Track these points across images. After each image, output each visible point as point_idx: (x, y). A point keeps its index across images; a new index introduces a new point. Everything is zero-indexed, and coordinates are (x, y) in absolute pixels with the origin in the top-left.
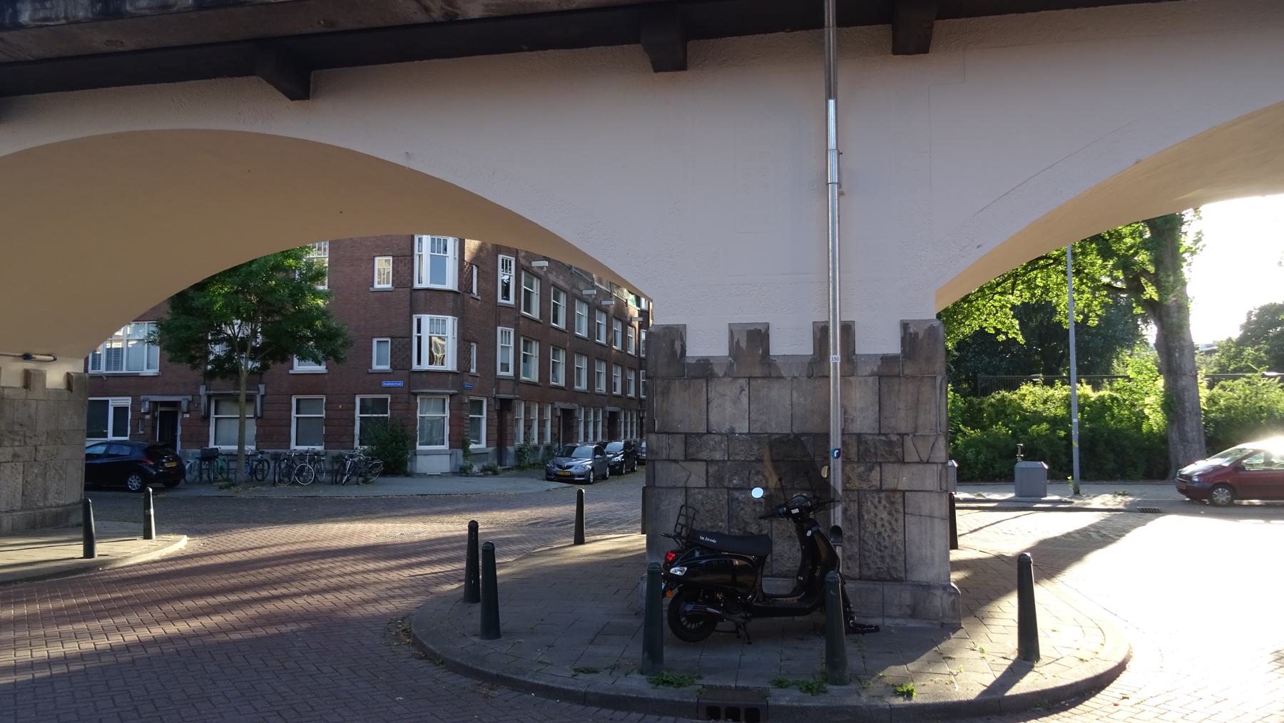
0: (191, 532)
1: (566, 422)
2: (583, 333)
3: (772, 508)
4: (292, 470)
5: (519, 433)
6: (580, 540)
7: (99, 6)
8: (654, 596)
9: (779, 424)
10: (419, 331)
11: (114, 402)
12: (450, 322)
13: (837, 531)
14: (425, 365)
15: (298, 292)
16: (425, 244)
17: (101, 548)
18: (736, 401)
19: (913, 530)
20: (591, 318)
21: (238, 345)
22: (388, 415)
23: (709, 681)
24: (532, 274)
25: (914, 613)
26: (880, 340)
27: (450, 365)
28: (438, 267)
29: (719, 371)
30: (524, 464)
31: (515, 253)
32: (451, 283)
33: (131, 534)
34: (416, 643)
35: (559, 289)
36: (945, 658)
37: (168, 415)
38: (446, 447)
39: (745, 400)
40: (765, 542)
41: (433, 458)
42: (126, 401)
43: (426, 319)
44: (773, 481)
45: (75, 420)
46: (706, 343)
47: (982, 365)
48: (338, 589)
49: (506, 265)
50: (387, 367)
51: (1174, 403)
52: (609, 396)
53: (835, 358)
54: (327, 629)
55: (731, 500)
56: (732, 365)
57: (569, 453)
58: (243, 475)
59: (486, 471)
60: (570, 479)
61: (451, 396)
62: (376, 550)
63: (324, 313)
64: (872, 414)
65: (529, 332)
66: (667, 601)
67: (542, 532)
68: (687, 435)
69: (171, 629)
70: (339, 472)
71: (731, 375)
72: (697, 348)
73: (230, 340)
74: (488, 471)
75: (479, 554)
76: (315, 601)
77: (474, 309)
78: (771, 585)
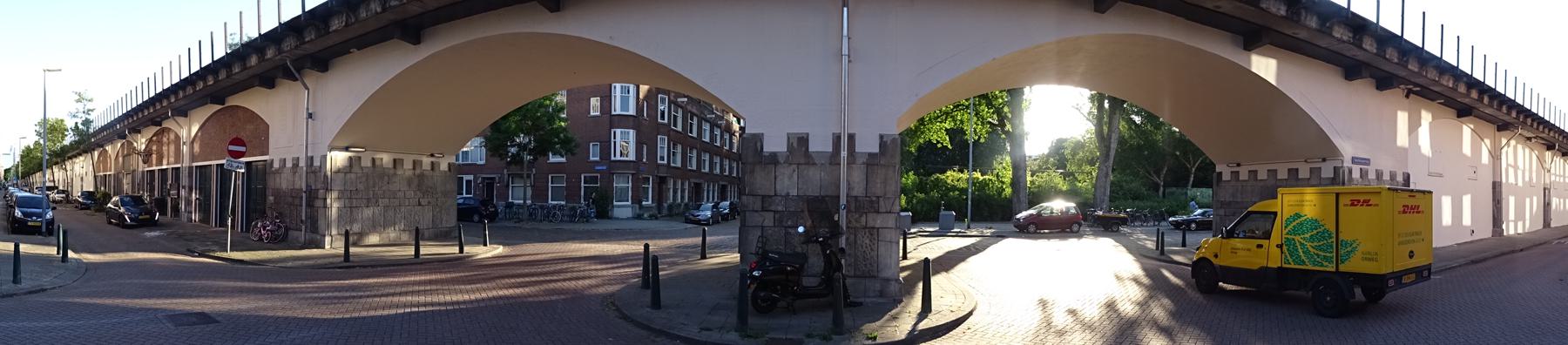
0: (504, 244)
1: (697, 192)
2: (707, 139)
3: (808, 238)
4: (549, 214)
5: (669, 197)
6: (704, 257)
8: (743, 287)
9: (813, 191)
11: (466, 178)
12: (632, 132)
13: (842, 250)
14: (618, 158)
15: (552, 118)
16: (618, 88)
17: (466, 249)
18: (790, 177)
19: (882, 250)
20: (712, 131)
21: (522, 147)
23: (772, 335)
24: (678, 105)
25: (882, 294)
26: (868, 145)
27: (632, 157)
28: (625, 101)
30: (673, 213)
31: (667, 93)
32: (632, 111)
33: (478, 243)
34: (618, 310)
35: (693, 115)
36: (895, 318)
37: (489, 184)
40: (804, 257)
41: (623, 209)
42: (471, 177)
43: (618, 131)
44: (809, 223)
45: (453, 186)
46: (775, 144)
47: (930, 159)
48: (578, 279)
49: (663, 101)
51: (1016, 182)
53: (844, 154)
54: (577, 297)
55: (787, 233)
57: (698, 208)
58: (526, 215)
59: (652, 217)
60: (698, 222)
62: (599, 258)
63: (564, 129)
64: (863, 185)
65: (676, 139)
66: (750, 291)
67: (682, 251)
69: (501, 293)
70: (573, 216)
71: (788, 162)
72: (768, 148)
73: (519, 145)
74: (653, 217)
75: (650, 262)
76: (573, 284)
77: (645, 126)
78: (808, 282)
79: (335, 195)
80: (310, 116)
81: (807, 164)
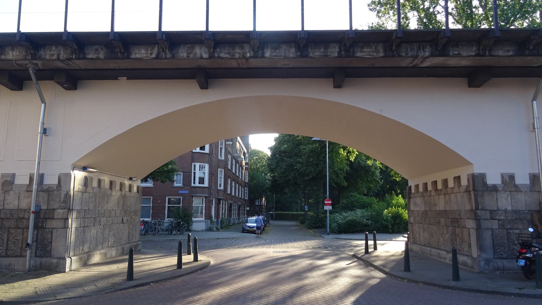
7: (299, 53)
10: (194, 170)
12: (207, 166)
14: (197, 184)
18: (507, 199)
22: (181, 205)
29: (500, 189)
38: (203, 219)
39: (510, 199)
41: (199, 223)
43: (197, 165)
50: (181, 185)
52: (235, 197)
53: (35, 186)
56: (504, 187)
61: (206, 197)
68: (491, 211)
71: (504, 190)
79: (74, 215)
80: (45, 131)
81: (517, 191)
